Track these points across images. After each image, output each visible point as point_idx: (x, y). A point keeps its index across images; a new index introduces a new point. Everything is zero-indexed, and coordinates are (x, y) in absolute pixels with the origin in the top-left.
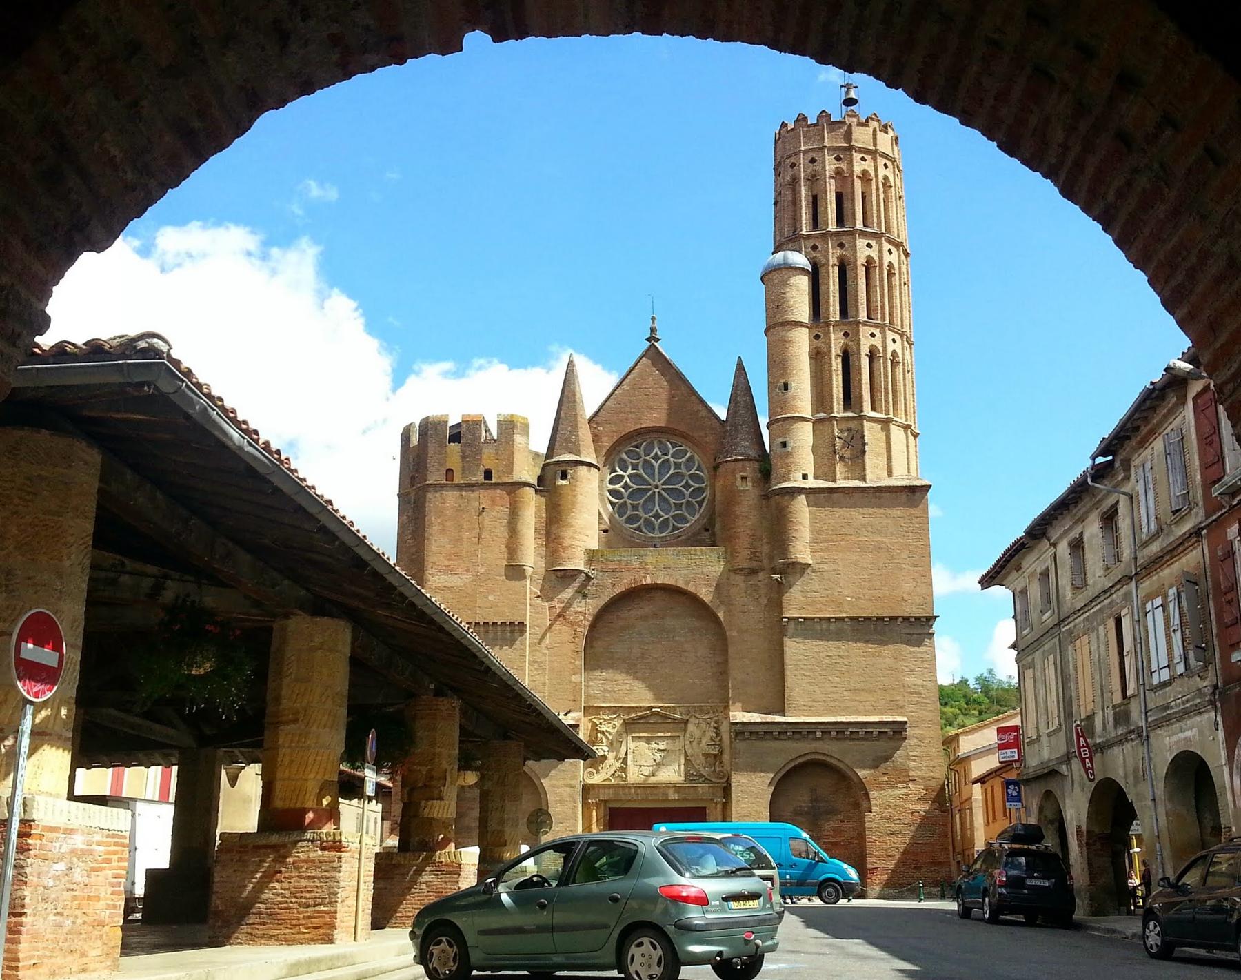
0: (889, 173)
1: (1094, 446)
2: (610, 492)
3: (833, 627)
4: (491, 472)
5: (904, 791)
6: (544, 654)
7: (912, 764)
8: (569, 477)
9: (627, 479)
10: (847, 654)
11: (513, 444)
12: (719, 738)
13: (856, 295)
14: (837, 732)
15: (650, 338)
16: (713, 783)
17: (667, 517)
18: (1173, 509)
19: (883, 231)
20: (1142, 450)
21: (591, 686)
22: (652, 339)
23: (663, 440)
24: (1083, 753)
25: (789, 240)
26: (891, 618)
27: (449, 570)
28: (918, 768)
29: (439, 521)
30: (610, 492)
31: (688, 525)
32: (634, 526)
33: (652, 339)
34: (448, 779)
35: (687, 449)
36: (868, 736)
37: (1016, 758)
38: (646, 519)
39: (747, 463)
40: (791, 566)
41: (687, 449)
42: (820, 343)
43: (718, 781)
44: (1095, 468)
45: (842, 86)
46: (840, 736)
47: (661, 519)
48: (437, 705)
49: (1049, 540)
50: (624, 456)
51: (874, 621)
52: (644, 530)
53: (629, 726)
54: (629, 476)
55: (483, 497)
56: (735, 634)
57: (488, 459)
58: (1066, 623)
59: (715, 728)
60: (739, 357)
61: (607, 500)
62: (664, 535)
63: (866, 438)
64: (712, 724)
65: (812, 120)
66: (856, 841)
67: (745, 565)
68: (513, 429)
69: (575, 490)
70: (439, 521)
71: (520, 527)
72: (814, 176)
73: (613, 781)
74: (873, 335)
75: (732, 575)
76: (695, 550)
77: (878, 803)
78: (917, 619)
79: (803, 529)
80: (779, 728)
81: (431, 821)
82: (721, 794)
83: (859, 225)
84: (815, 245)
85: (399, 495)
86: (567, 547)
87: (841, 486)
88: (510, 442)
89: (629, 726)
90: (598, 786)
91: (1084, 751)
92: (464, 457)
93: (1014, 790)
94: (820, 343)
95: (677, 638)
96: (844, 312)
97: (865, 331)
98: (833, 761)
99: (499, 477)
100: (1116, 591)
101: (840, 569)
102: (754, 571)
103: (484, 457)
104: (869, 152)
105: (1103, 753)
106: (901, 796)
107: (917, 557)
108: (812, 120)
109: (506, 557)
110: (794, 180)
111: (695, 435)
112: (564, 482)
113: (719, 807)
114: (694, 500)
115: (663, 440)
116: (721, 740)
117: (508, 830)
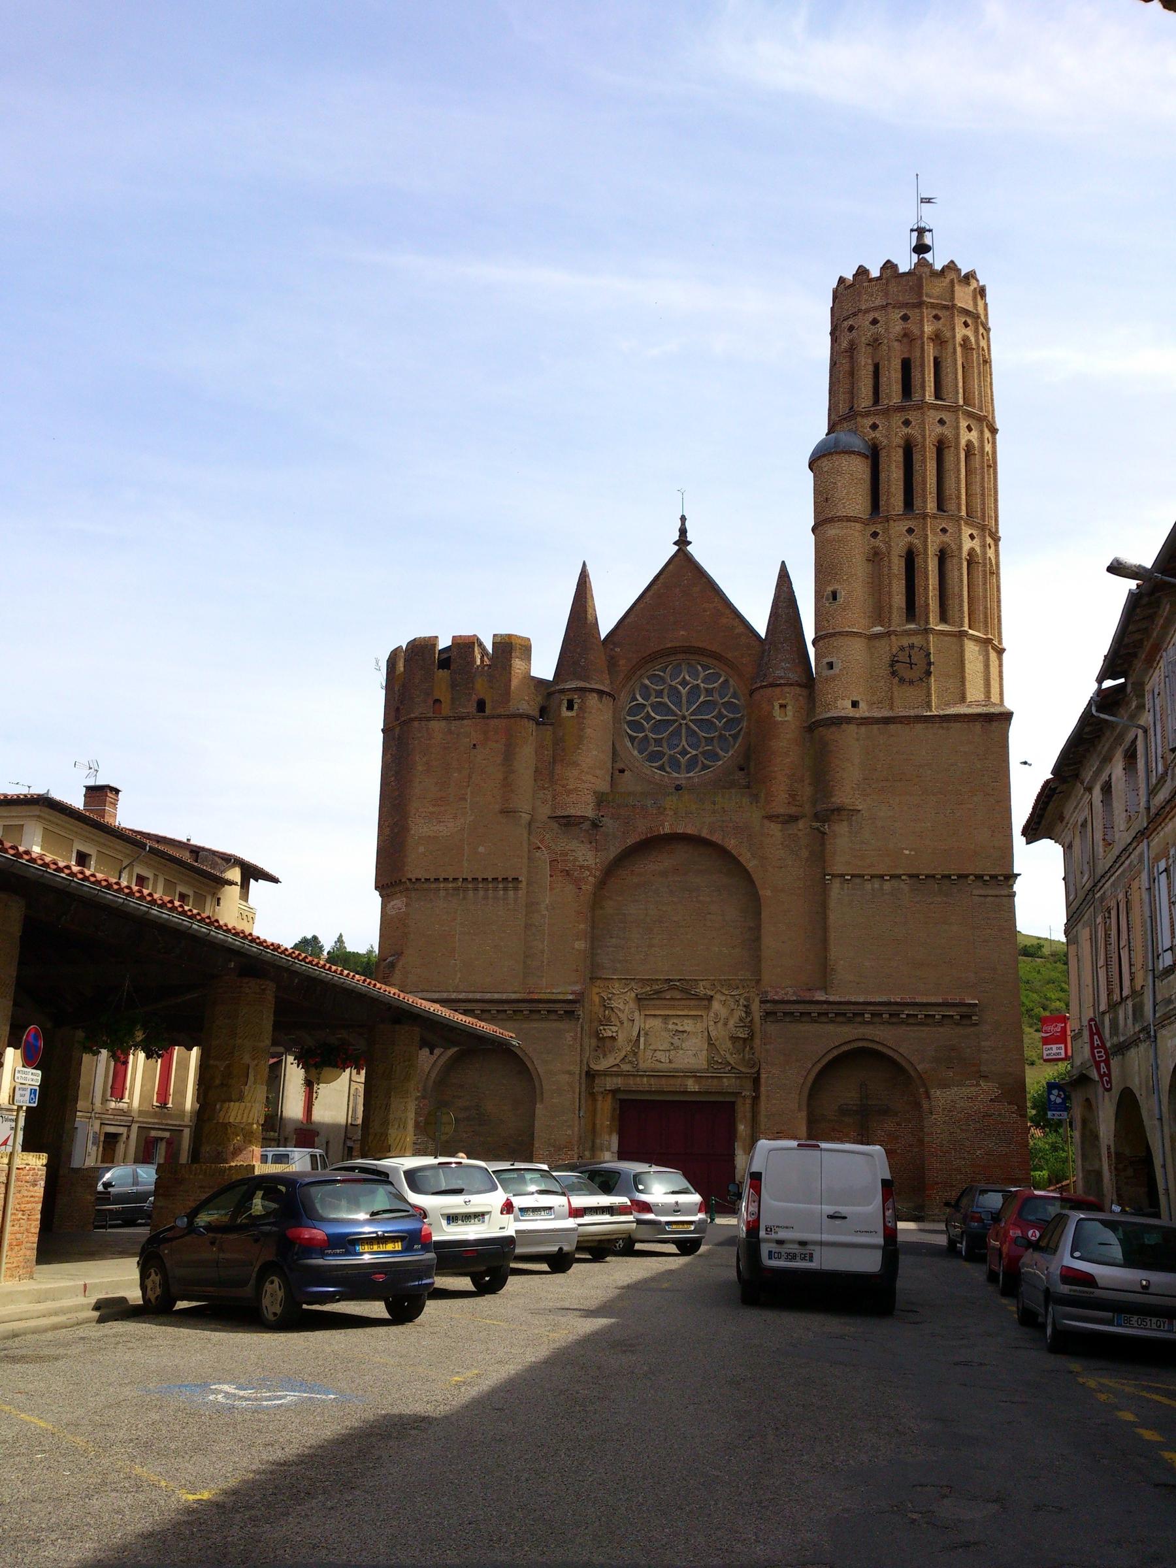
0: (969, 332)
1: (1097, 664)
2: (629, 723)
3: (887, 886)
4: (485, 703)
6: (544, 916)
7: (984, 1056)
11: (510, 669)
13: (924, 483)
14: (890, 1015)
15: (678, 541)
16: (741, 1072)
17: (694, 752)
18: (1171, 747)
19: (961, 402)
20: (1152, 671)
22: (683, 541)
24: (1097, 1055)
25: (844, 419)
26: (960, 876)
29: (424, 760)
31: (721, 762)
32: (657, 764)
33: (683, 541)
34: (251, 1078)
36: (930, 1021)
37: (1063, 1056)
38: (670, 755)
39: (787, 689)
41: (722, 673)
42: (878, 542)
43: (749, 1071)
44: (1102, 695)
45: (912, 230)
46: (894, 1020)
47: (688, 756)
48: (241, 987)
49: (1082, 783)
50: (647, 682)
52: (668, 769)
54: (652, 705)
56: (768, 893)
57: (481, 688)
58: (1098, 888)
59: (745, 1006)
60: (783, 562)
62: (691, 774)
63: (932, 656)
64: (742, 1001)
65: (875, 273)
67: (782, 811)
70: (424, 760)
72: (876, 340)
74: (944, 530)
75: (766, 822)
77: (940, 1105)
81: (226, 1125)
82: (749, 1084)
83: (929, 397)
84: (874, 423)
85: (383, 730)
87: (901, 714)
88: (507, 667)
90: (605, 1073)
91: (1098, 1052)
92: (453, 685)
93: (1059, 1096)
94: (878, 542)
95: (701, 898)
96: (909, 503)
98: (885, 1050)
100: (1133, 850)
102: (793, 819)
105: (1123, 1055)
108: (875, 273)
110: (852, 345)
111: (729, 655)
112: (570, 714)
113: (749, 1101)
114: (727, 733)
116: (751, 1021)
117: (393, 1132)
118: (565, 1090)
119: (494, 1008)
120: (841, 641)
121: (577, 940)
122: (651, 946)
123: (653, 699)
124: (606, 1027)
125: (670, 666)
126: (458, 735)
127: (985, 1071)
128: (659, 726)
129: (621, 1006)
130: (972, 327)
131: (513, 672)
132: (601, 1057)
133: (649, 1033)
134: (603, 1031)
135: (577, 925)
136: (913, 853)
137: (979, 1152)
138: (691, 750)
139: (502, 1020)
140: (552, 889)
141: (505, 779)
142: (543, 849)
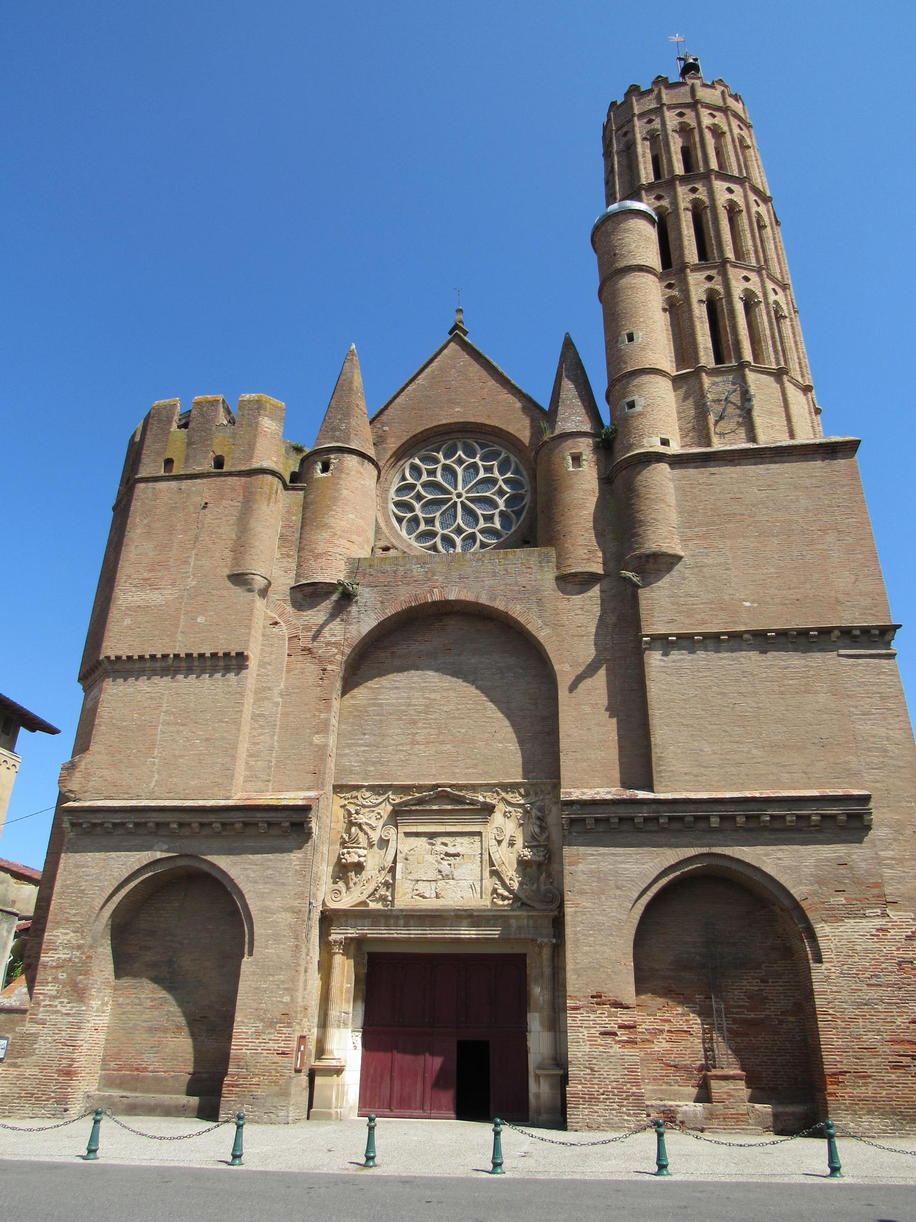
5: (879, 922)
7: (887, 872)
8: (332, 467)
9: (419, 488)
10: (751, 689)
11: (256, 426)
12: (544, 836)
21: (346, 755)
23: (469, 441)
27: (149, 584)
28: (901, 880)
29: (145, 522)
30: (398, 504)
35: (501, 449)
40: (651, 560)
46: (751, 825)
50: (417, 461)
51: (795, 637)
53: (397, 815)
55: (203, 489)
59: (539, 818)
61: (391, 514)
66: (792, 1019)
68: (259, 409)
69: (338, 484)
70: (145, 522)
71: (253, 524)
73: (373, 905)
76: (506, 554)
77: (832, 946)
78: (866, 631)
79: (667, 509)
80: (645, 812)
86: (321, 554)
89: (397, 815)
92: (190, 444)
97: (735, 276)
99: (233, 465)
101: (729, 561)
103: (216, 441)
104: (719, 109)
106: (874, 932)
107: (851, 540)
109: (229, 564)
113: (546, 953)
115: (469, 441)
116: (548, 838)
118: (285, 936)
119: (196, 819)
120: (645, 378)
121: (317, 733)
122: (414, 743)
123: (425, 478)
124: (350, 850)
125: (445, 446)
126: (188, 495)
127: (891, 894)
128: (432, 486)
129: (373, 822)
130: (718, 279)
131: (259, 429)
132: (344, 889)
133: (409, 857)
134: (347, 856)
135: (317, 714)
136: (756, 605)
137: (899, 1019)
138: (467, 529)
139: (206, 837)
140: (288, 671)
141: (239, 538)
142: (282, 624)
